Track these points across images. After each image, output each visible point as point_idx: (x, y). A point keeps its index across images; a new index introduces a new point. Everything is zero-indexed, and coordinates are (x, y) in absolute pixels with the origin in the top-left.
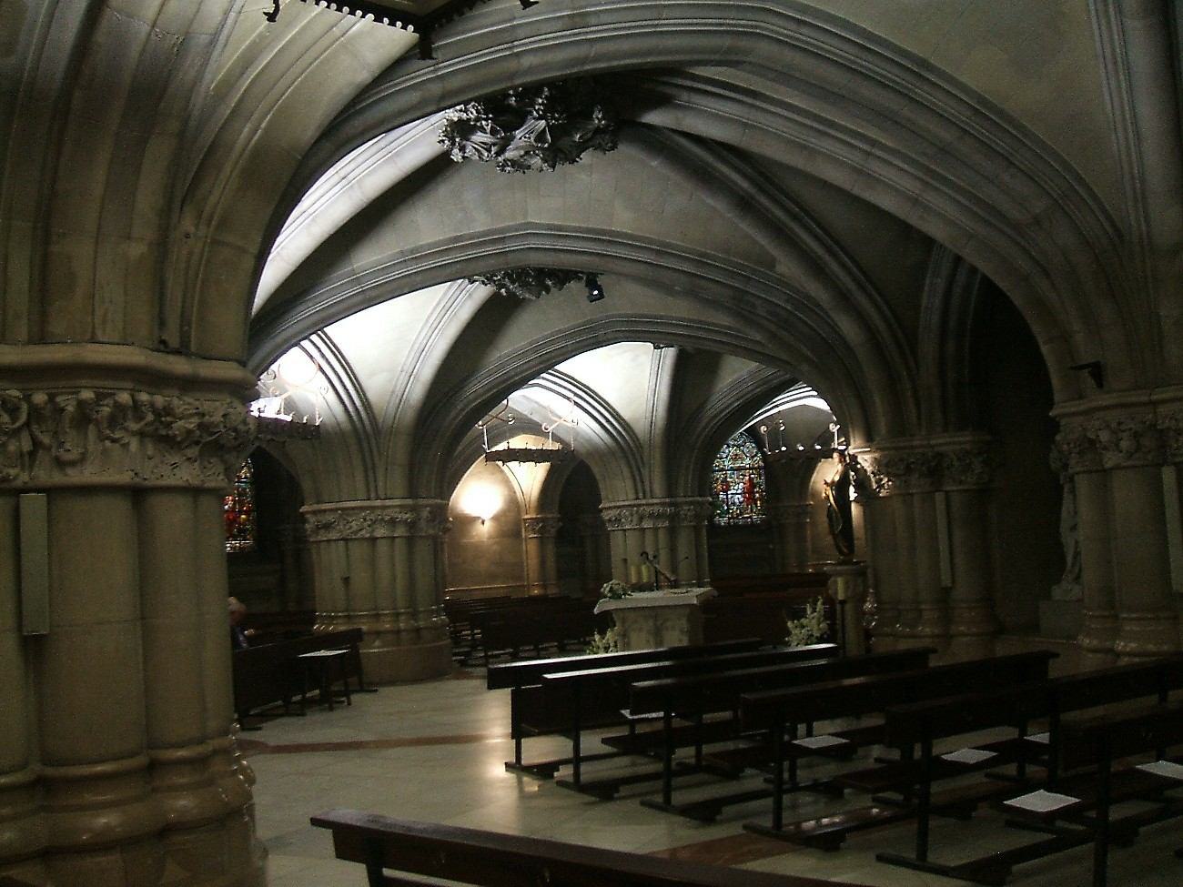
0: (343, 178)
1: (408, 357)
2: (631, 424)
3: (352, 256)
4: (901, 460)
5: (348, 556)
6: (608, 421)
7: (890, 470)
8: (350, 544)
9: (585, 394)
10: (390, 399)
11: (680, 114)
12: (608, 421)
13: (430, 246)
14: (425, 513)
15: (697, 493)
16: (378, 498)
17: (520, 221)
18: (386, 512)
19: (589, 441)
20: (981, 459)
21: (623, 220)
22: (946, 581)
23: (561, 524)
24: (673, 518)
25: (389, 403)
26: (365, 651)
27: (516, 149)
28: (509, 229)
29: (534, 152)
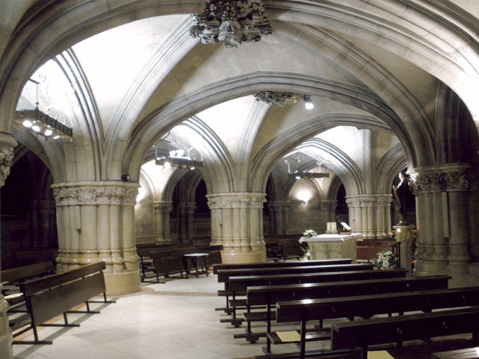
0: (164, 55)
1: (242, 133)
2: (357, 163)
3: (183, 88)
4: (427, 176)
5: (222, 216)
6: (345, 161)
7: (421, 182)
8: (82, 208)
9: (334, 149)
10: (237, 151)
11: (294, 15)
12: (345, 161)
13: (217, 83)
14: (254, 199)
15: (385, 192)
16: (234, 192)
17: (255, 70)
18: (237, 197)
19: (339, 169)
20: (197, 175)
21: (299, 68)
22: (446, 235)
23: (338, 204)
24: (375, 202)
25: (237, 153)
26: (228, 254)
27: (222, 35)
28: (250, 74)
29: (230, 36)
